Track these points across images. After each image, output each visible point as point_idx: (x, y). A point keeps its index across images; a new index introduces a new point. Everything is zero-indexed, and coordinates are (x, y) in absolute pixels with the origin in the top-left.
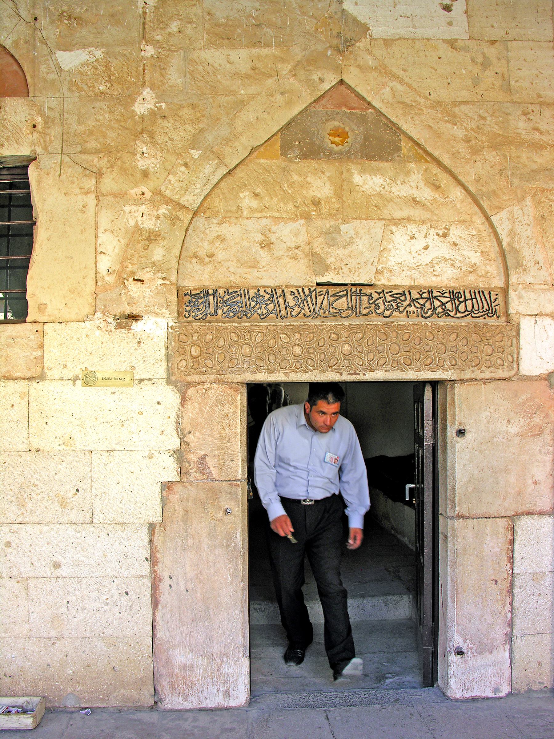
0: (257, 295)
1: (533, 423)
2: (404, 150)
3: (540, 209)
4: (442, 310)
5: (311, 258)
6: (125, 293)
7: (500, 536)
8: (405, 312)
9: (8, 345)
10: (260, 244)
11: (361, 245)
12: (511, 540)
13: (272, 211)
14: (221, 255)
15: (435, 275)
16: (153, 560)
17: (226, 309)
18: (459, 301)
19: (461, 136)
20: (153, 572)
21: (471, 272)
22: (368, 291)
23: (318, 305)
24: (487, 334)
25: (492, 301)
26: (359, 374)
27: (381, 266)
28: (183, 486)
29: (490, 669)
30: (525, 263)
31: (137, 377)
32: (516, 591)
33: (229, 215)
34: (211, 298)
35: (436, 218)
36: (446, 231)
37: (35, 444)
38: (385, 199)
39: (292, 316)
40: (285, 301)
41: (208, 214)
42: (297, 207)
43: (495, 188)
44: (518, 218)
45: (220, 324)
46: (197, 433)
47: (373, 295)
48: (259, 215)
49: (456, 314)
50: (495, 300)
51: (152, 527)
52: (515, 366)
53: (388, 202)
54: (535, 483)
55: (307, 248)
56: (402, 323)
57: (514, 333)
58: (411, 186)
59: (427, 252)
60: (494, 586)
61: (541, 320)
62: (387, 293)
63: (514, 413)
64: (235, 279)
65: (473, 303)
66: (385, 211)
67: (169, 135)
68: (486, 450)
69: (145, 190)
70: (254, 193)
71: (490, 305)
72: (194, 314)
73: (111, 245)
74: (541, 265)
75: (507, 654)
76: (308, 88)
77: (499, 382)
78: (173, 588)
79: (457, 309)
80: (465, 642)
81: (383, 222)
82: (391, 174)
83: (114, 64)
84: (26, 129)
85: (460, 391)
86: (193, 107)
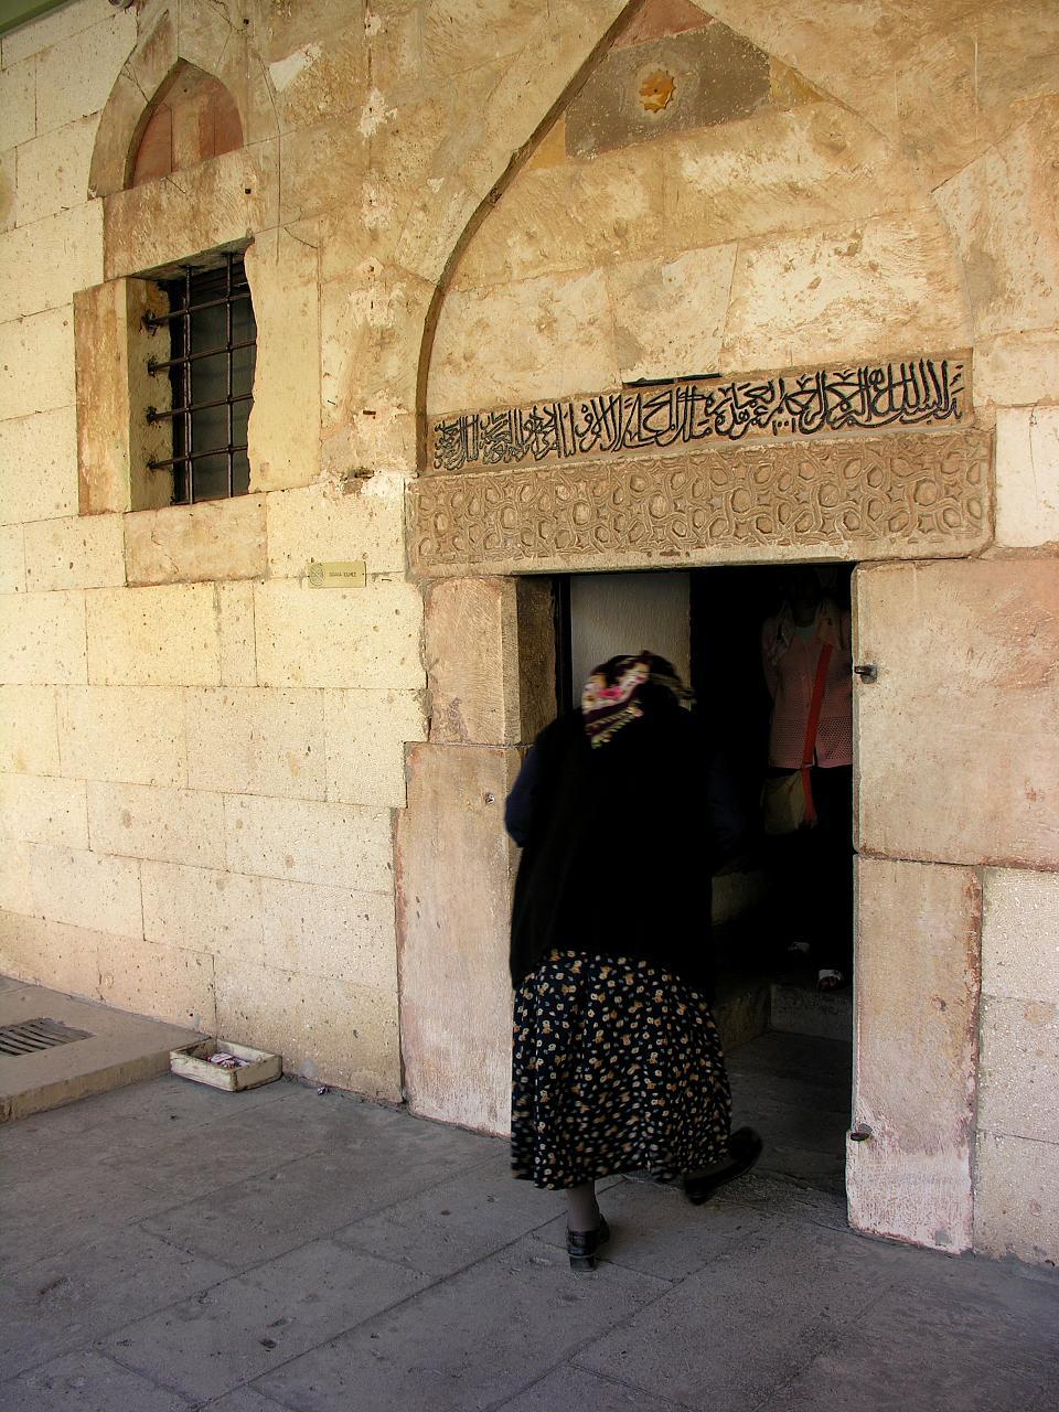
0: (534, 417)
1: (1027, 657)
2: (775, 88)
3: (1049, 148)
4: (842, 414)
5: (613, 337)
6: (354, 436)
7: (952, 907)
8: (771, 423)
9: (231, 530)
10: (539, 326)
11: (696, 299)
12: (975, 918)
13: (554, 262)
14: (483, 354)
15: (831, 340)
16: (397, 868)
17: (489, 447)
18: (876, 389)
19: (872, 24)
20: (397, 888)
21: (905, 324)
22: (706, 388)
23: (624, 427)
24: (927, 458)
25: (950, 380)
26: (678, 554)
27: (732, 336)
28: (431, 751)
29: (929, 1188)
30: (1009, 285)
31: (370, 570)
32: (986, 1032)
33: (493, 280)
34: (470, 430)
35: (834, 218)
36: (854, 241)
37: (263, 678)
38: (738, 198)
39: (583, 451)
40: (572, 423)
41: (465, 285)
42: (591, 246)
43: (944, 125)
44: (995, 182)
45: (471, 475)
46: (446, 662)
47: (715, 397)
48: (535, 273)
49: (869, 419)
50: (955, 379)
51: (394, 812)
52: (985, 525)
53: (744, 202)
54: (1032, 796)
55: (608, 320)
56: (753, 448)
57: (984, 451)
58: (786, 160)
59: (815, 293)
60: (939, 1013)
61: (1046, 417)
62: (740, 389)
63: (984, 633)
64: (502, 393)
65: (906, 391)
66: (739, 223)
67: (403, 161)
68: (920, 713)
69: (374, 262)
70: (528, 234)
71: (942, 391)
72: (446, 460)
73: (337, 357)
74: (1048, 283)
75: (965, 1166)
76: (595, 15)
77: (951, 564)
78: (422, 918)
79: (873, 409)
80: (877, 1119)
81: (734, 246)
82: (750, 142)
83: (334, 63)
84: (240, 197)
85: (866, 585)
86: (432, 102)
